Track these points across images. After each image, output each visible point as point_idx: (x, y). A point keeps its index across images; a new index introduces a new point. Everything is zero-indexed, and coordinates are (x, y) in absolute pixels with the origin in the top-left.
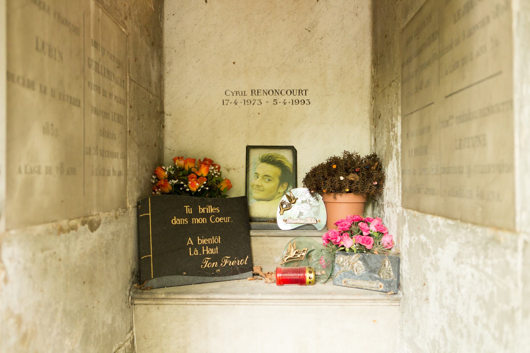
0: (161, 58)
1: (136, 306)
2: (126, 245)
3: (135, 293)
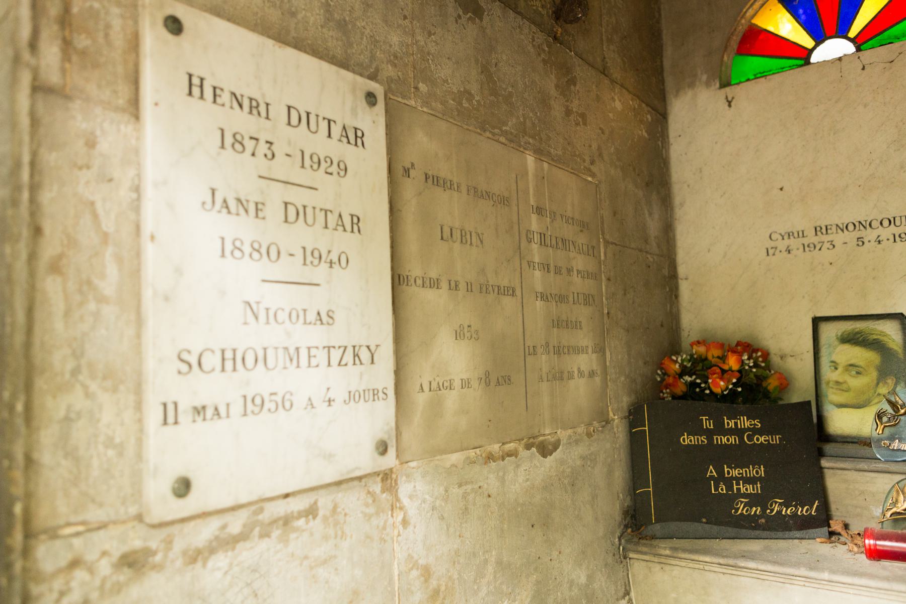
0: (666, 201)
1: (632, 561)
2: (610, 472)
3: (628, 541)
